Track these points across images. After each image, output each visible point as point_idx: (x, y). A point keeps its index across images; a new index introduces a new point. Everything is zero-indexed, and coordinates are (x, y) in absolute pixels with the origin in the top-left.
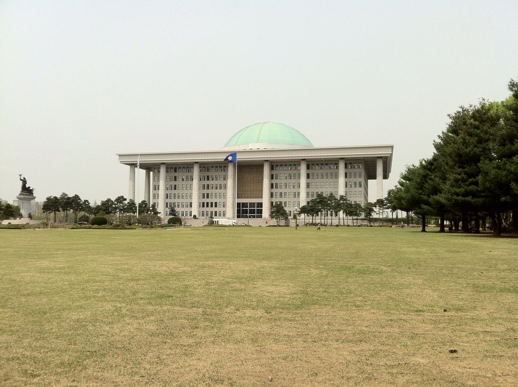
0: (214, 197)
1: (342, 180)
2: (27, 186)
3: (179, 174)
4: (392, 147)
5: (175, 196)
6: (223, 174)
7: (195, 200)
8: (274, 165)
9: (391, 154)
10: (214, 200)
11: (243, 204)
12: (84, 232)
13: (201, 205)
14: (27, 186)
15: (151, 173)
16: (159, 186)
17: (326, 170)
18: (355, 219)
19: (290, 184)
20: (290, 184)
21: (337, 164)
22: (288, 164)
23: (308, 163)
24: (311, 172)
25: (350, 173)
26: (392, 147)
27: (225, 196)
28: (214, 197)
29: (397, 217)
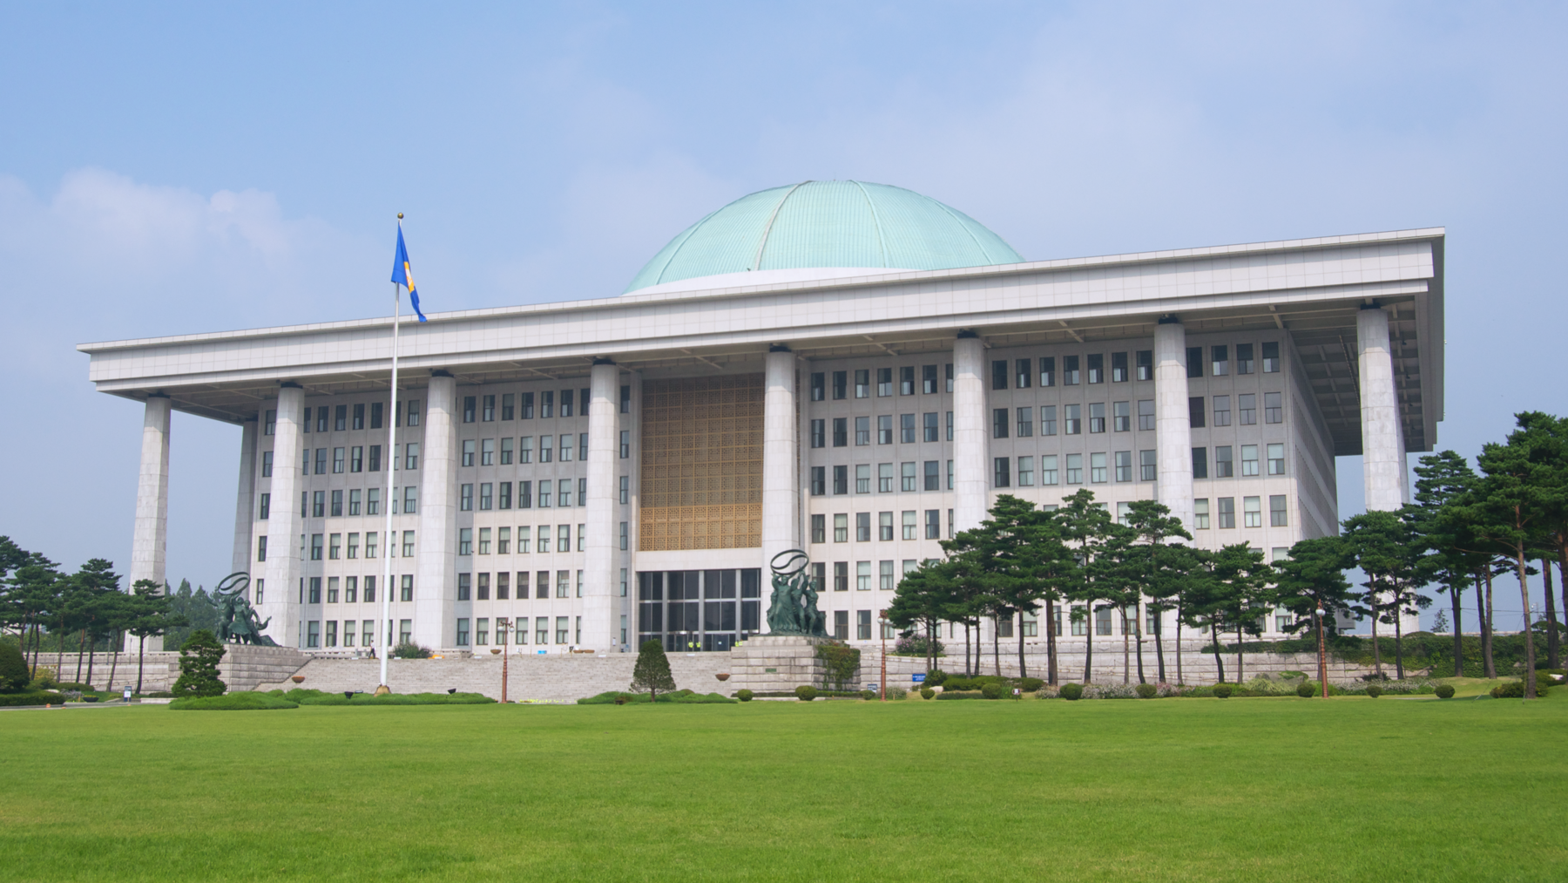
0: (532, 546)
3: (860, 404)
4: (1436, 245)
5: (352, 548)
6: (920, 405)
7: (432, 569)
8: (827, 370)
9: (1436, 283)
10: (533, 563)
11: (675, 576)
12: (559, 696)
13: (572, 580)
16: (583, 482)
17: (1085, 390)
18: (1232, 649)
19: (863, 473)
20: (863, 473)
21: (752, 388)
22: (896, 365)
23: (1000, 356)
24: (1013, 399)
25: (862, 420)
26: (1436, 245)
28: (532, 546)
29: (1485, 625)
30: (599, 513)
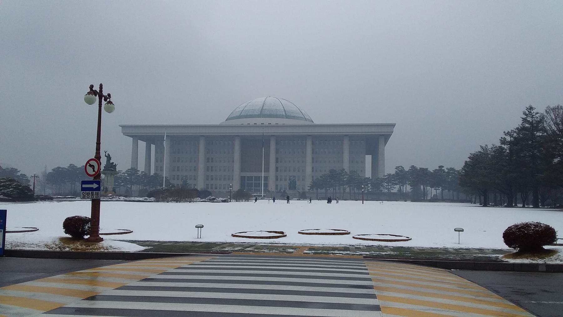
1: (346, 156)
2: (111, 162)
8: (279, 139)
14: (111, 162)
15: (153, 147)
27: (196, 169)
30: (237, 166)
